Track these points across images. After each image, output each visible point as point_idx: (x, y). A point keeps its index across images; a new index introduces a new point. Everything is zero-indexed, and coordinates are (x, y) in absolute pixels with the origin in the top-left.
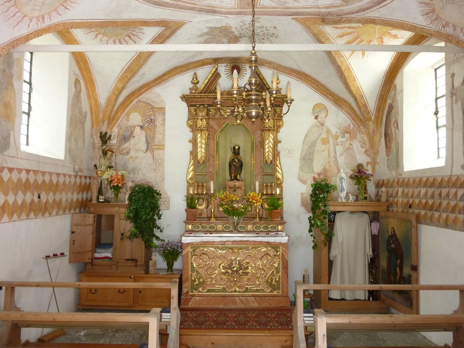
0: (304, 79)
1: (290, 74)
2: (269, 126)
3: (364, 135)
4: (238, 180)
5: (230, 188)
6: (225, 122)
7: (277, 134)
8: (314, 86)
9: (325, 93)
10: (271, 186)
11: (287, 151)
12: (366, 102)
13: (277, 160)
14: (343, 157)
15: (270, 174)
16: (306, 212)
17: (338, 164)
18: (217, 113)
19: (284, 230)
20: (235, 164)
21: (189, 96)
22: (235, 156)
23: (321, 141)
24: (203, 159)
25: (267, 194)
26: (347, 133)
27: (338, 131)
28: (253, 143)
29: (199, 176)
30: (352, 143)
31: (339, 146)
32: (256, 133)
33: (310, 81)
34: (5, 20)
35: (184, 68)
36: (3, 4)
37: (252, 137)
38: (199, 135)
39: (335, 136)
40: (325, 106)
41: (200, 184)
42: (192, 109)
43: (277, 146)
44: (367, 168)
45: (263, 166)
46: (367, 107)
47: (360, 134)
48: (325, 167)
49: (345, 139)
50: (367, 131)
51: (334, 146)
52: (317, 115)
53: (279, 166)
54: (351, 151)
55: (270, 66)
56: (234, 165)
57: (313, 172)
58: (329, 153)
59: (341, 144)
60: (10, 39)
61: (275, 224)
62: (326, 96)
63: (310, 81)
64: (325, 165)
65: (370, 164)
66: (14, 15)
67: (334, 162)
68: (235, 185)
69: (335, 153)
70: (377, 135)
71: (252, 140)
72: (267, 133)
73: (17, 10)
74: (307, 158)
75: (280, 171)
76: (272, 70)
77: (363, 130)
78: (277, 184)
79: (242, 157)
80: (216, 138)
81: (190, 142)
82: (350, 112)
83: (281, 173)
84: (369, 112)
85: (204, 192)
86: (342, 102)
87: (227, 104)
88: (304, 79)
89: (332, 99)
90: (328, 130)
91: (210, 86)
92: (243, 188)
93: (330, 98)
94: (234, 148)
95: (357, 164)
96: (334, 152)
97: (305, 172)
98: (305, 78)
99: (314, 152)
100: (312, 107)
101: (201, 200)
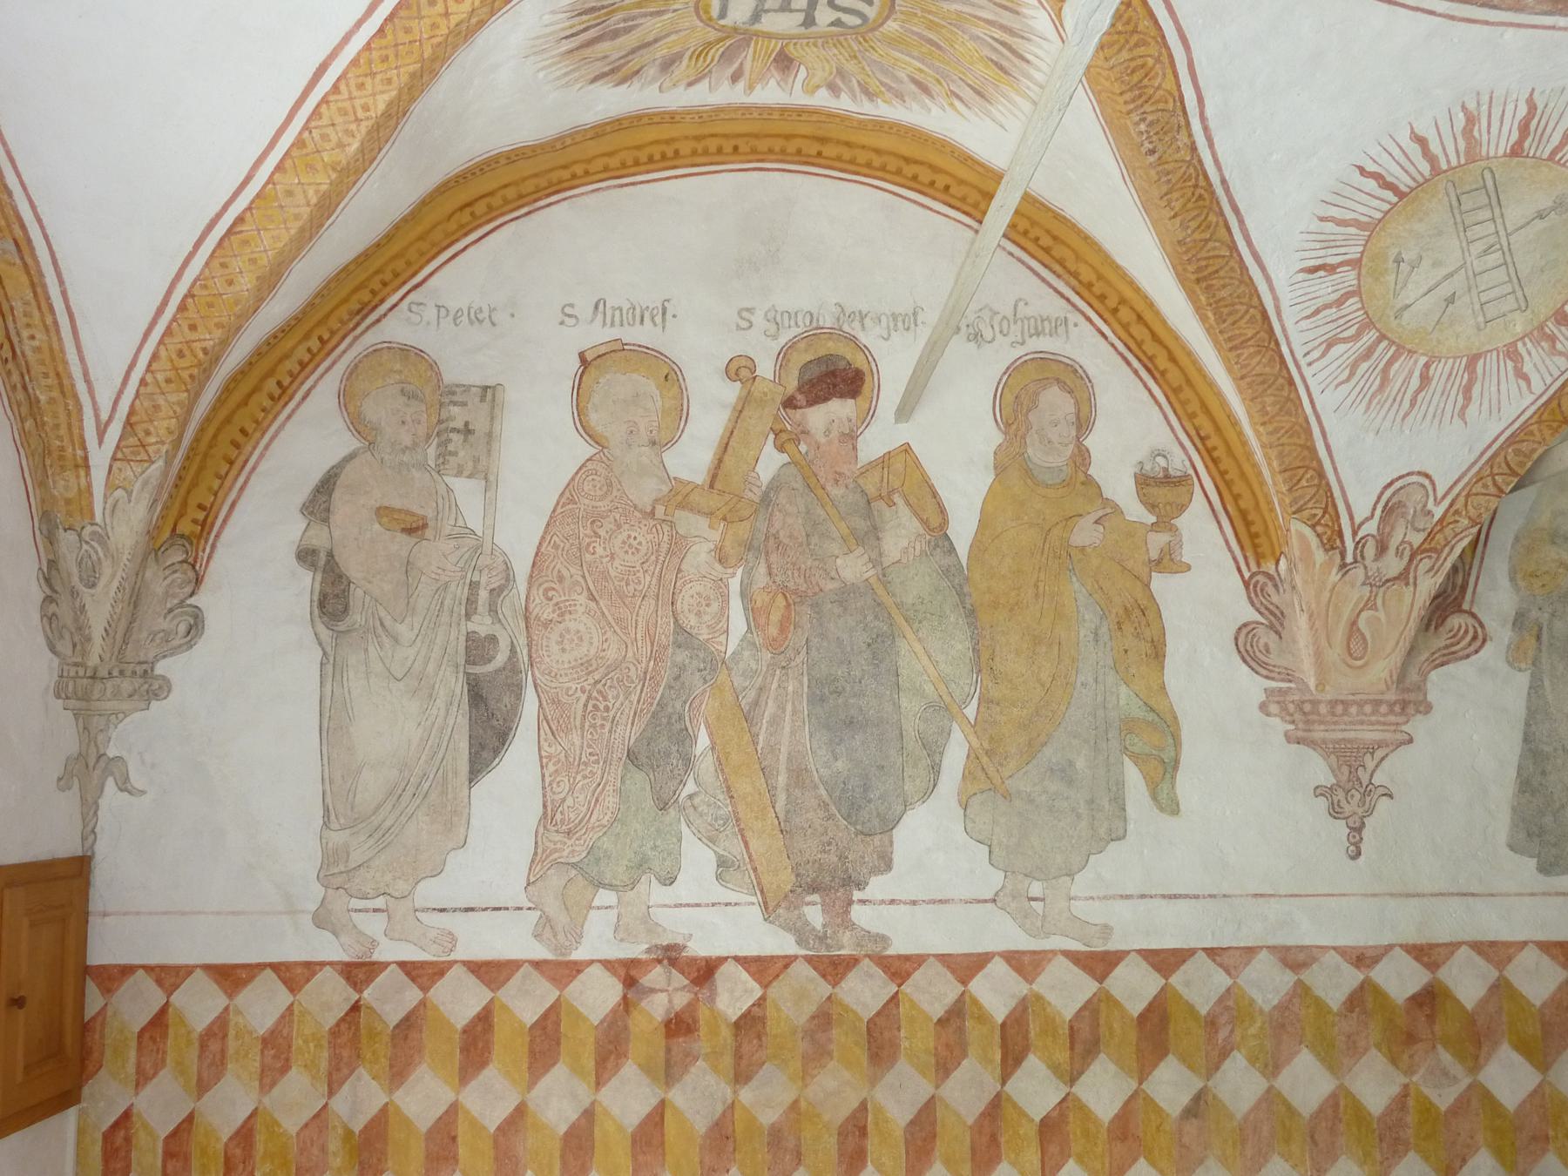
34: (1402, 413)
36: (1352, 374)
60: (1472, 458)
66: (1425, 379)
73: (1423, 360)
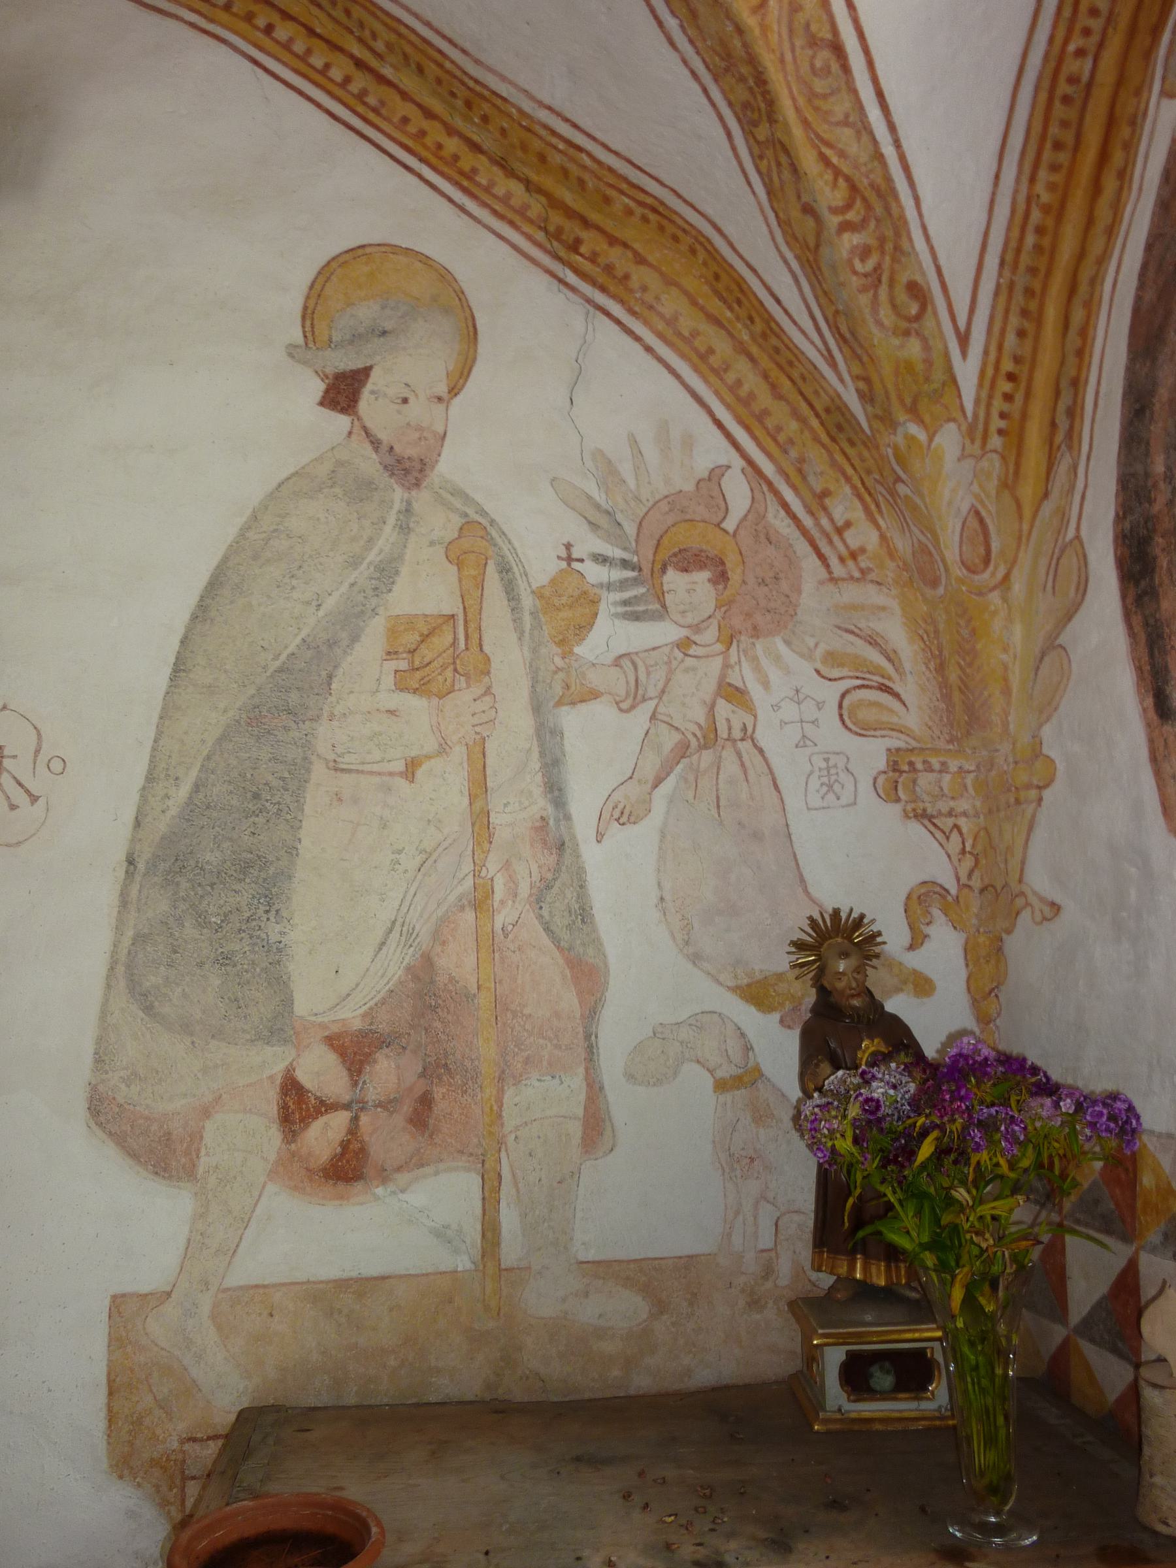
3: (872, 595)
8: (336, 74)
9: (452, 145)
12: (888, 150)
14: (645, 833)
17: (583, 914)
23: (391, 654)
26: (689, 561)
27: (588, 543)
30: (744, 676)
31: (601, 710)
39: (548, 598)
40: (445, 276)
44: (914, 961)
46: (900, 226)
47: (833, 580)
48: (427, 960)
49: (664, 633)
50: (902, 545)
51: (537, 708)
54: (730, 766)
58: (479, 786)
59: (616, 681)
62: (465, 180)
64: (437, 935)
65: (951, 906)
67: (538, 900)
69: (555, 790)
70: (1018, 587)
74: (211, 857)
77: (864, 536)
82: (723, 347)
84: (916, 290)
86: (626, 234)
89: (522, 212)
90: (467, 527)
93: (505, 200)
95: (795, 924)
96: (534, 782)
97: (186, 1028)
100: (301, 277)
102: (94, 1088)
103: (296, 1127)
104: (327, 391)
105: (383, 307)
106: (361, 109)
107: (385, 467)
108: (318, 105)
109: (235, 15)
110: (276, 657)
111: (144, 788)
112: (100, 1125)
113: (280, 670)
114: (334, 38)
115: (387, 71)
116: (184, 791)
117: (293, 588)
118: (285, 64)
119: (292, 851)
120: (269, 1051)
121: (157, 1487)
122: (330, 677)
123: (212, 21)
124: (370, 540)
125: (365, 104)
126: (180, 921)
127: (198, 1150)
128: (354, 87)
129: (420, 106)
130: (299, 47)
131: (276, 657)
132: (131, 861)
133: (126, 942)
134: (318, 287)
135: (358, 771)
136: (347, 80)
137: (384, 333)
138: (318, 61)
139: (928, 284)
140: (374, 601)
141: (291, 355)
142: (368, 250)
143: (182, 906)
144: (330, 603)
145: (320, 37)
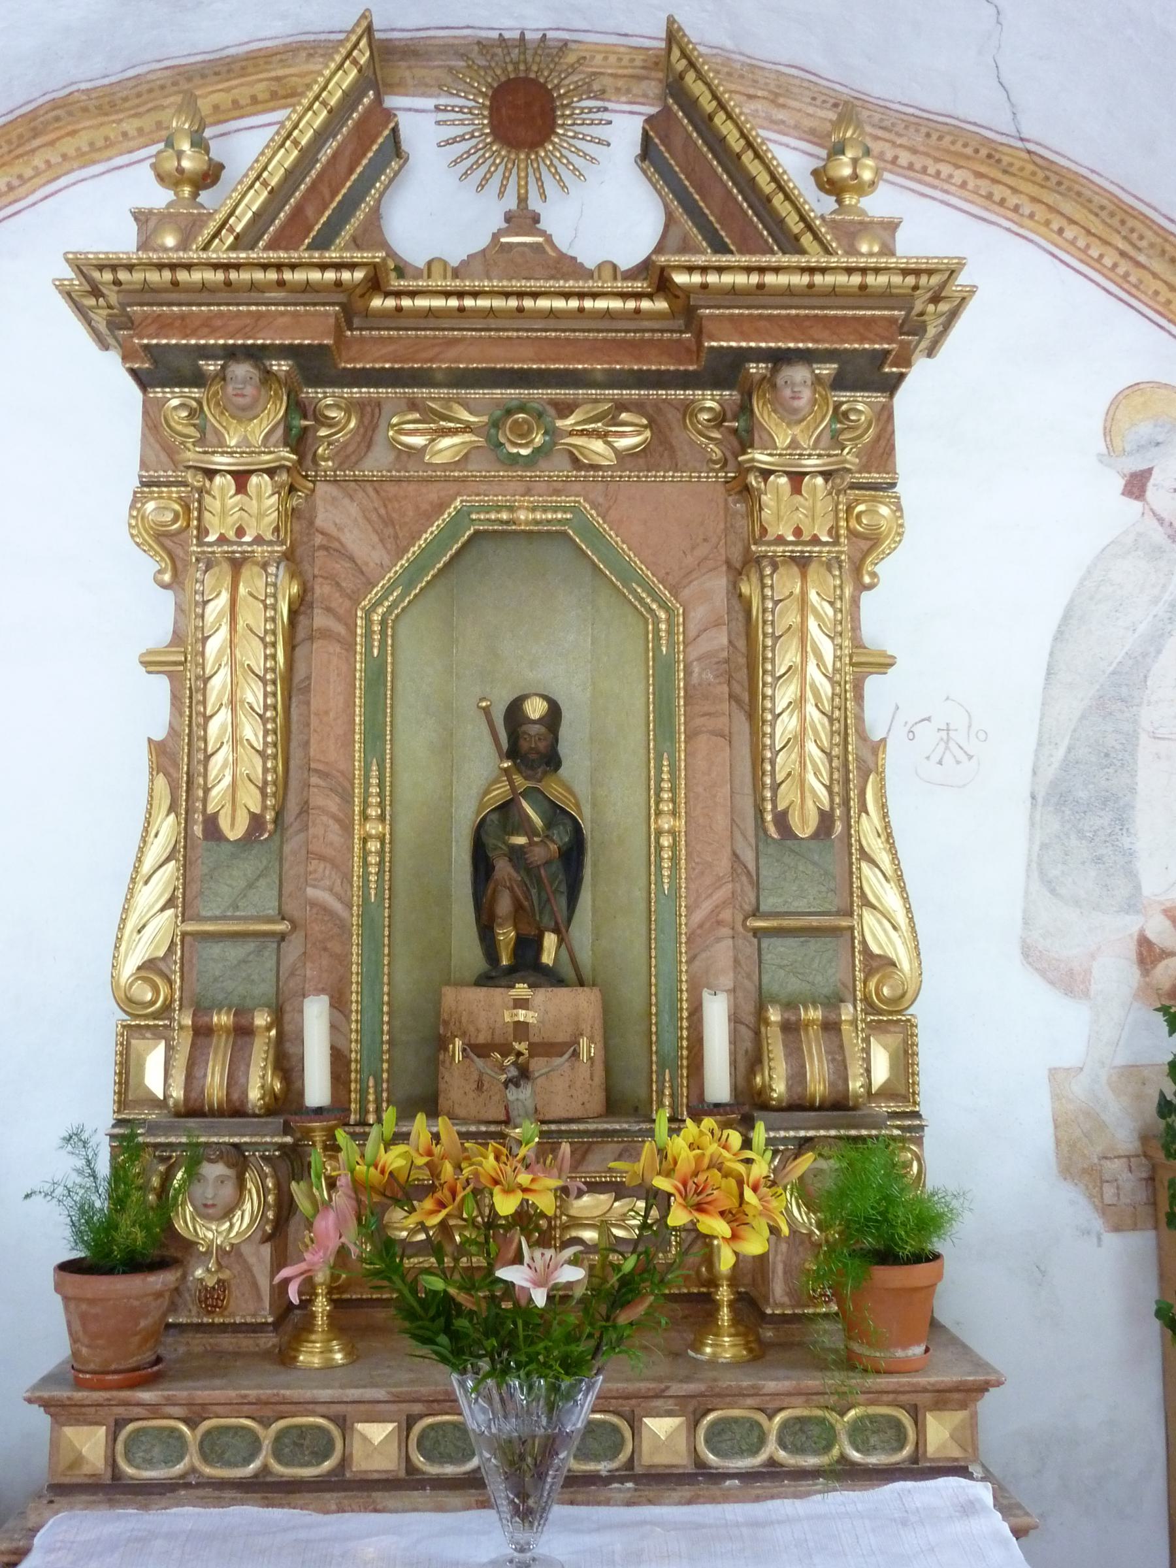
0: (1026, 210)
1: (924, 170)
2: (798, 532)
4: (551, 978)
5: (478, 1050)
6: (441, 507)
7: (855, 602)
8: (1108, 262)
10: (831, 1027)
11: (928, 735)
13: (863, 809)
15: (814, 921)
16: (1098, 1223)
18: (379, 438)
19: (976, 1459)
20: (521, 840)
21: (130, 268)
22: (518, 780)
24: (251, 800)
25: (798, 1105)
28: (664, 670)
29: (216, 950)
32: (686, 593)
33: (1072, 221)
35: (137, 123)
37: (657, 621)
38: (218, 605)
41: (222, 1019)
42: (174, 399)
43: (859, 698)
45: (748, 857)
52: (1140, 465)
53: (884, 859)
55: (780, 115)
56: (517, 855)
57: (1133, 904)
61: (894, 1396)
63: (1072, 221)
68: (521, 1028)
71: (657, 648)
72: (786, 582)
74: (1082, 795)
75: (890, 898)
76: (794, 142)
78: (870, 1007)
79: (582, 789)
80: (368, 634)
81: (150, 664)
83: (901, 919)
85: (254, 1094)
87: (453, 352)
88: (1026, 210)
91: (310, 212)
92: (588, 1048)
94: (514, 712)
98: (1035, 200)
99: (1130, 741)
101: (214, 1170)
102: (1024, 941)
103: (1149, 967)
104: (1126, 486)
105: (1155, 426)
106: (1126, 286)
107: (1169, 536)
108: (1098, 285)
109: (1038, 222)
110: (1110, 664)
111: (1036, 750)
112: (1030, 964)
113: (1113, 673)
114: (1104, 236)
115: (1142, 258)
116: (1061, 752)
117: (1118, 619)
118: (1073, 256)
119: (1133, 791)
120: (1128, 918)
121: (1087, 1186)
122: (1146, 677)
123: (1022, 226)
124: (1164, 586)
125: (1128, 282)
126: (1067, 835)
127: (1090, 981)
128: (1121, 270)
129: (1165, 282)
130: (1081, 243)
131: (1110, 664)
132: (1033, 797)
133: (1036, 848)
134: (1111, 413)
135: (1169, 739)
136: (1115, 265)
137: (1158, 444)
138: (1095, 253)
139: (607, 1503)
140: (1170, 627)
141: (1101, 461)
142: (1141, 386)
143: (1068, 826)
144: (1142, 628)
145: (1094, 235)
